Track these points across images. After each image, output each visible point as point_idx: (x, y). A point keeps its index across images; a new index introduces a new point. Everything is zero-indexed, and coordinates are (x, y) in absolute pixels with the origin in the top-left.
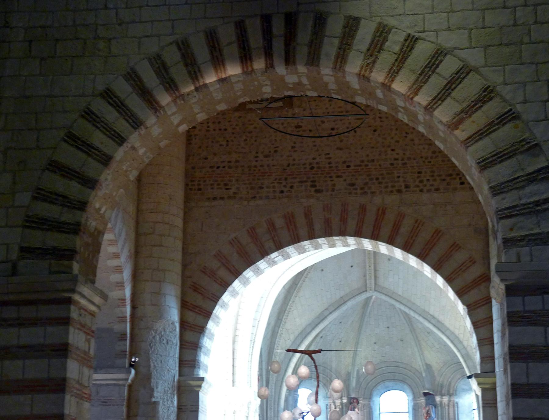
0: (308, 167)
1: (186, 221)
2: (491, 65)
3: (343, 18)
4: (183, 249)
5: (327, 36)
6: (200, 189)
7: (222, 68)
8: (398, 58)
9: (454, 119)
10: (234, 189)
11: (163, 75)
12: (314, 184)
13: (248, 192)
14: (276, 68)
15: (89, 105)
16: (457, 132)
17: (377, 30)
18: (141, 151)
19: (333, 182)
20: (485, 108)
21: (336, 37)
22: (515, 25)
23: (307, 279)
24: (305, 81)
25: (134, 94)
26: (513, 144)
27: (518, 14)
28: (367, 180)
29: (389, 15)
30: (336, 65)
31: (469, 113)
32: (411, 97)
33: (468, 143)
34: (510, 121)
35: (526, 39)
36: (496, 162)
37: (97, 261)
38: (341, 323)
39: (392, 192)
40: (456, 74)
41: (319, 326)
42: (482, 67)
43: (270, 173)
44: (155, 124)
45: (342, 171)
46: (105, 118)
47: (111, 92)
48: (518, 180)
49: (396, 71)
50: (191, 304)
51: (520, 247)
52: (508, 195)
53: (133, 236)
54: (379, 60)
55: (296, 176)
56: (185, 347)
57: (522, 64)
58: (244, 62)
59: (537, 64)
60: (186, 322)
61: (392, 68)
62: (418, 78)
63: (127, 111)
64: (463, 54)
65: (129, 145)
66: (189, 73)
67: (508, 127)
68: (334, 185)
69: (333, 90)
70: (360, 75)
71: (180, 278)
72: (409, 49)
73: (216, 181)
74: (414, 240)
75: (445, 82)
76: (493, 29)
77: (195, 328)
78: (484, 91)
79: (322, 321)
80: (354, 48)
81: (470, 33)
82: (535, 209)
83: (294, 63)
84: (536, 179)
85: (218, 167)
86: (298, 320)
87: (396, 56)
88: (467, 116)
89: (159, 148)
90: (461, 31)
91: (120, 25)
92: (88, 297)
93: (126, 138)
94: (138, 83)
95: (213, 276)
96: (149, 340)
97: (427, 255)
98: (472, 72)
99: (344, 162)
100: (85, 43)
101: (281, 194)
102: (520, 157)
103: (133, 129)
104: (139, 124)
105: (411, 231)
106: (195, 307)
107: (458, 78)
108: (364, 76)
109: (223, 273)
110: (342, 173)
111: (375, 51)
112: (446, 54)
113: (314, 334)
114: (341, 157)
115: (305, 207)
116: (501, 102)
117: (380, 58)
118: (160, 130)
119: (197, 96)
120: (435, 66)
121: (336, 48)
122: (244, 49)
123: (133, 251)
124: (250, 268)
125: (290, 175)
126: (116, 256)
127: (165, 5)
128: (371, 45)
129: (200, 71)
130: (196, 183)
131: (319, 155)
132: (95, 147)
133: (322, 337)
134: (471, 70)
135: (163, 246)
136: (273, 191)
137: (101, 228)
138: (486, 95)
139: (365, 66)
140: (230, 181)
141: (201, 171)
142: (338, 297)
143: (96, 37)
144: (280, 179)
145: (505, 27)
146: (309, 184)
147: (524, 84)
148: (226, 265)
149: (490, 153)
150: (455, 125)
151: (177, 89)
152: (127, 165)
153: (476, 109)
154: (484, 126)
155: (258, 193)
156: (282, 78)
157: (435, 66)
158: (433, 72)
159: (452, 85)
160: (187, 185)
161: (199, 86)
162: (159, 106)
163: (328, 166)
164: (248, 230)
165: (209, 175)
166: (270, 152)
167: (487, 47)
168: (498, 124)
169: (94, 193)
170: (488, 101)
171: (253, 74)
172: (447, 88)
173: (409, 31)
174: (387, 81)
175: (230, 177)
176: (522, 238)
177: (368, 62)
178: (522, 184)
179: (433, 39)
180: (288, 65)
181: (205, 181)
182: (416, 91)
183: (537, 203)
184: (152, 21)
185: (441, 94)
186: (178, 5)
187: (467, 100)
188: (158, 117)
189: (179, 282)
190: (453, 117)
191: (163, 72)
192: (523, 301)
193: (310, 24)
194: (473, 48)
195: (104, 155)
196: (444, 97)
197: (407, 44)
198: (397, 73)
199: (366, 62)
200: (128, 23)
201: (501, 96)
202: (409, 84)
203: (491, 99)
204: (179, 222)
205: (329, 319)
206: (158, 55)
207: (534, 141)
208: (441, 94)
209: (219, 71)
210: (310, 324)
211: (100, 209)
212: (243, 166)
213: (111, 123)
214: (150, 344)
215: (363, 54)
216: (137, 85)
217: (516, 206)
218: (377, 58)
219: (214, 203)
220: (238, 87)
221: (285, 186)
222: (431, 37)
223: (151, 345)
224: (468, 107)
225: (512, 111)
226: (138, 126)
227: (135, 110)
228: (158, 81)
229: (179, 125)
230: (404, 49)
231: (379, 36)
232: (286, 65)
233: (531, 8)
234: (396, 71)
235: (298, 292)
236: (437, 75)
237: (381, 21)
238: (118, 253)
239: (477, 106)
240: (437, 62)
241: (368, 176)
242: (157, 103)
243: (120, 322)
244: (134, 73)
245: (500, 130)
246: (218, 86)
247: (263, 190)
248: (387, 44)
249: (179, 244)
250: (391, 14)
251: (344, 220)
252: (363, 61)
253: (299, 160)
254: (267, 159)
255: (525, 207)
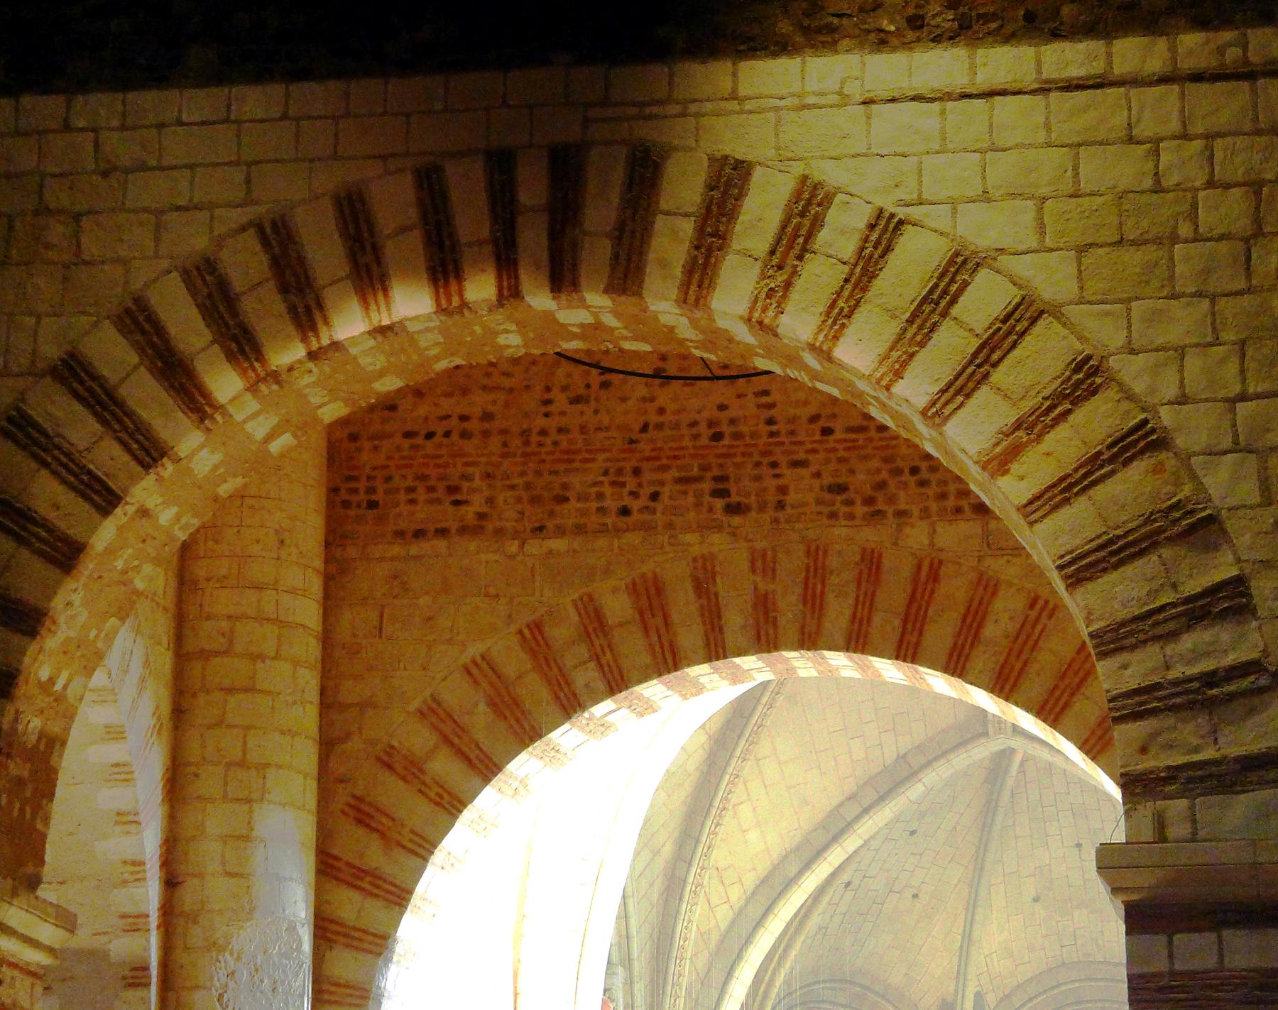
0: (706, 433)
1: (330, 604)
2: (1093, 298)
3: (706, 163)
4: (323, 691)
5: (661, 212)
6: (372, 505)
7: (381, 297)
8: (851, 274)
9: (997, 444)
10: (477, 504)
11: (222, 317)
12: (721, 486)
13: (522, 513)
14: (527, 298)
15: (23, 400)
16: (1003, 482)
17: (797, 195)
18: (166, 517)
19: (780, 482)
20: (1078, 416)
21: (686, 215)
22: (1158, 189)
23: (781, 698)
24: (610, 320)
25: (142, 368)
26: (1150, 517)
27: (1165, 158)
28: (884, 475)
29: (827, 154)
30: (686, 293)
31: (1036, 431)
32: (884, 383)
33: (1034, 512)
34: (1142, 452)
35: (1185, 230)
36: (1105, 565)
37: (46, 820)
38: (913, 833)
39: (958, 510)
40: (1004, 321)
41: (814, 866)
42: (1071, 303)
43: (588, 451)
44: (202, 446)
45: (809, 446)
46: (64, 438)
47: (79, 362)
48: (1161, 616)
49: (846, 310)
50: (349, 865)
51: (1165, 799)
52: (1138, 655)
53: (165, 661)
54: (799, 281)
55: (669, 462)
56: (326, 997)
57: (1174, 297)
58: (441, 283)
59: (1213, 299)
60: (332, 921)
61: (834, 303)
62: (905, 330)
63: (126, 419)
64: (1023, 267)
65: (131, 509)
66: (292, 310)
67: (1139, 467)
68: (783, 490)
69: (692, 341)
70: (749, 320)
71: (313, 785)
72: (879, 251)
73: (423, 478)
74: (1026, 663)
75: (975, 343)
76: (1100, 200)
77: (360, 940)
78: (1077, 369)
79: (835, 839)
80: (735, 245)
81: (1040, 210)
82: (1205, 693)
83: (575, 286)
84: (1209, 612)
85: (430, 435)
86: (753, 836)
87: (846, 269)
88: (1032, 436)
89: (216, 499)
90: (1018, 203)
91: (105, 174)
92: (21, 930)
93: (119, 492)
94: (155, 339)
95: (418, 778)
96: (218, 985)
97: (1066, 706)
98: (1046, 315)
99: (814, 419)
100: (11, 228)
101: (624, 519)
102: (1166, 552)
103: (139, 469)
104: (155, 454)
105: (1018, 635)
106: (361, 873)
107: (1009, 333)
108: (760, 323)
109: (444, 766)
110: (808, 452)
111: (791, 254)
112: (978, 265)
113: (810, 882)
114: (806, 403)
115: (695, 560)
116: (1119, 400)
117: (804, 274)
118: (218, 457)
119: (315, 370)
120: (948, 297)
121: (686, 245)
122: (441, 246)
123: (166, 709)
124: (530, 749)
125: (648, 459)
126: (114, 733)
127: (227, 120)
128: (778, 240)
129: (321, 307)
130: (362, 485)
131: (739, 396)
132: (38, 518)
133: (848, 885)
134: (1042, 312)
135: (260, 691)
136: (598, 509)
137: (55, 728)
138: (1081, 382)
139: (763, 295)
140: (464, 477)
141: (376, 448)
142: (890, 754)
143: (43, 210)
144: (620, 472)
145: (1131, 195)
146: (707, 486)
147: (1181, 352)
148: (456, 740)
149: (1092, 540)
150: (1000, 463)
151: (260, 357)
152: (126, 556)
153: (1053, 420)
154: (1075, 465)
155: (552, 514)
156: (549, 317)
157: (948, 297)
158: (944, 315)
159: (992, 351)
160: (333, 490)
161: (320, 348)
162: (211, 406)
163: (764, 429)
164: (520, 632)
165: (403, 458)
166: (588, 386)
167: (1082, 250)
168: (1111, 460)
169: (33, 648)
170: (1086, 398)
171: (466, 312)
172: (978, 361)
173: (880, 202)
174: (821, 338)
175: (466, 464)
176: (1173, 774)
177: (773, 285)
178: (1171, 626)
179: (944, 224)
180: (559, 291)
181: (388, 479)
182: (897, 366)
183: (1210, 679)
184: (191, 167)
185: (965, 375)
186: (261, 121)
187: (1033, 393)
188: (209, 430)
189: (312, 802)
190: (994, 440)
191: (221, 308)
192: (1170, 943)
193: (618, 175)
194: (1047, 251)
195: (60, 540)
196: (971, 385)
197: (874, 236)
198: (849, 317)
199: (767, 285)
200: (127, 171)
201: (1120, 384)
202: (882, 348)
203: (1094, 391)
204: (309, 612)
205: (859, 831)
206: (208, 261)
207: (1205, 508)
208: (965, 375)
209: (373, 307)
210: (798, 849)
211: (52, 681)
212: (504, 432)
213: (80, 452)
214: (221, 996)
215: (759, 264)
216: (153, 346)
217: (1156, 687)
218: (795, 273)
219: (424, 547)
220: (430, 342)
221: (634, 494)
222: (937, 217)
223: (225, 999)
224: (1033, 413)
225: (1149, 426)
226: (155, 460)
227: (144, 414)
228: (207, 336)
229: (270, 437)
230: (867, 252)
231: (802, 215)
232: (552, 291)
233: (1198, 144)
234: (846, 310)
235: (753, 743)
236: (952, 323)
237: (806, 172)
238: (121, 726)
239: (1057, 412)
240: (954, 288)
241: (886, 460)
242: (206, 395)
243: (128, 931)
244: (144, 311)
245: (1119, 476)
246: (372, 343)
247: (566, 506)
248: (823, 236)
249: (310, 681)
250: (834, 154)
251: (813, 601)
252: (758, 283)
253: (678, 412)
254: (580, 407)
255: (1178, 689)
